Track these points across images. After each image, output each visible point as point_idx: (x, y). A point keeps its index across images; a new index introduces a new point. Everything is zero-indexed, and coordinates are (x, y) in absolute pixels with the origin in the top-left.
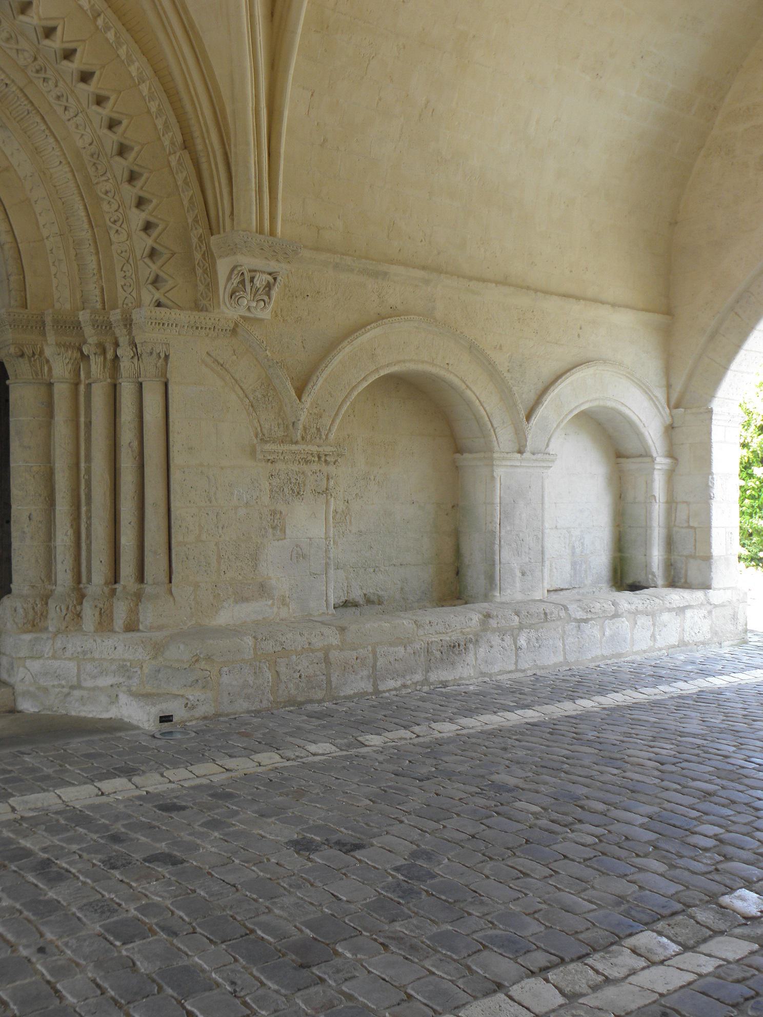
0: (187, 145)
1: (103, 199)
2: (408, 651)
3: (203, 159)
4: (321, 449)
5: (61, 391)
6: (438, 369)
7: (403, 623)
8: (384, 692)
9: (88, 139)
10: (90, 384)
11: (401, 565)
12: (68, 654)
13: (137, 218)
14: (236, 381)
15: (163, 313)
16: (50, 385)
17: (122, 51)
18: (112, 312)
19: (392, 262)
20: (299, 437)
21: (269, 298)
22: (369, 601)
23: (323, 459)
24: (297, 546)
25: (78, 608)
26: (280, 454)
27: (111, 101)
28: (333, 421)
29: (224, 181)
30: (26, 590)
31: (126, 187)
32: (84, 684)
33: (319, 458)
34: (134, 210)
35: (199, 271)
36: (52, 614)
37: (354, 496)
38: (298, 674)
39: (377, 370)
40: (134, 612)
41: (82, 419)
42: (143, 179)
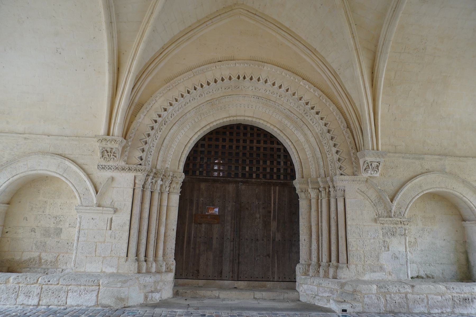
0: (348, 127)
1: (324, 145)
2: (443, 298)
3: (354, 130)
4: (401, 220)
5: (314, 201)
6: (449, 190)
7: (440, 287)
8: (433, 314)
9: (319, 129)
10: (322, 200)
11: (441, 264)
12: (315, 284)
13: (334, 150)
14: (368, 197)
15: (342, 177)
16: (310, 200)
17: (328, 104)
18: (327, 178)
19: (425, 154)
20: (393, 216)
21: (378, 170)
22: (428, 277)
23: (402, 223)
24: (394, 254)
25: (318, 269)
26: (385, 221)
27: (325, 118)
28: (406, 210)
29: (361, 135)
30: (303, 262)
31: (330, 141)
32: (319, 295)
33: (401, 223)
34: (333, 148)
35: (354, 163)
36: (311, 271)
37: (418, 236)
38: (395, 302)
39: (423, 191)
40: (336, 272)
41: (320, 210)
42: (335, 138)
